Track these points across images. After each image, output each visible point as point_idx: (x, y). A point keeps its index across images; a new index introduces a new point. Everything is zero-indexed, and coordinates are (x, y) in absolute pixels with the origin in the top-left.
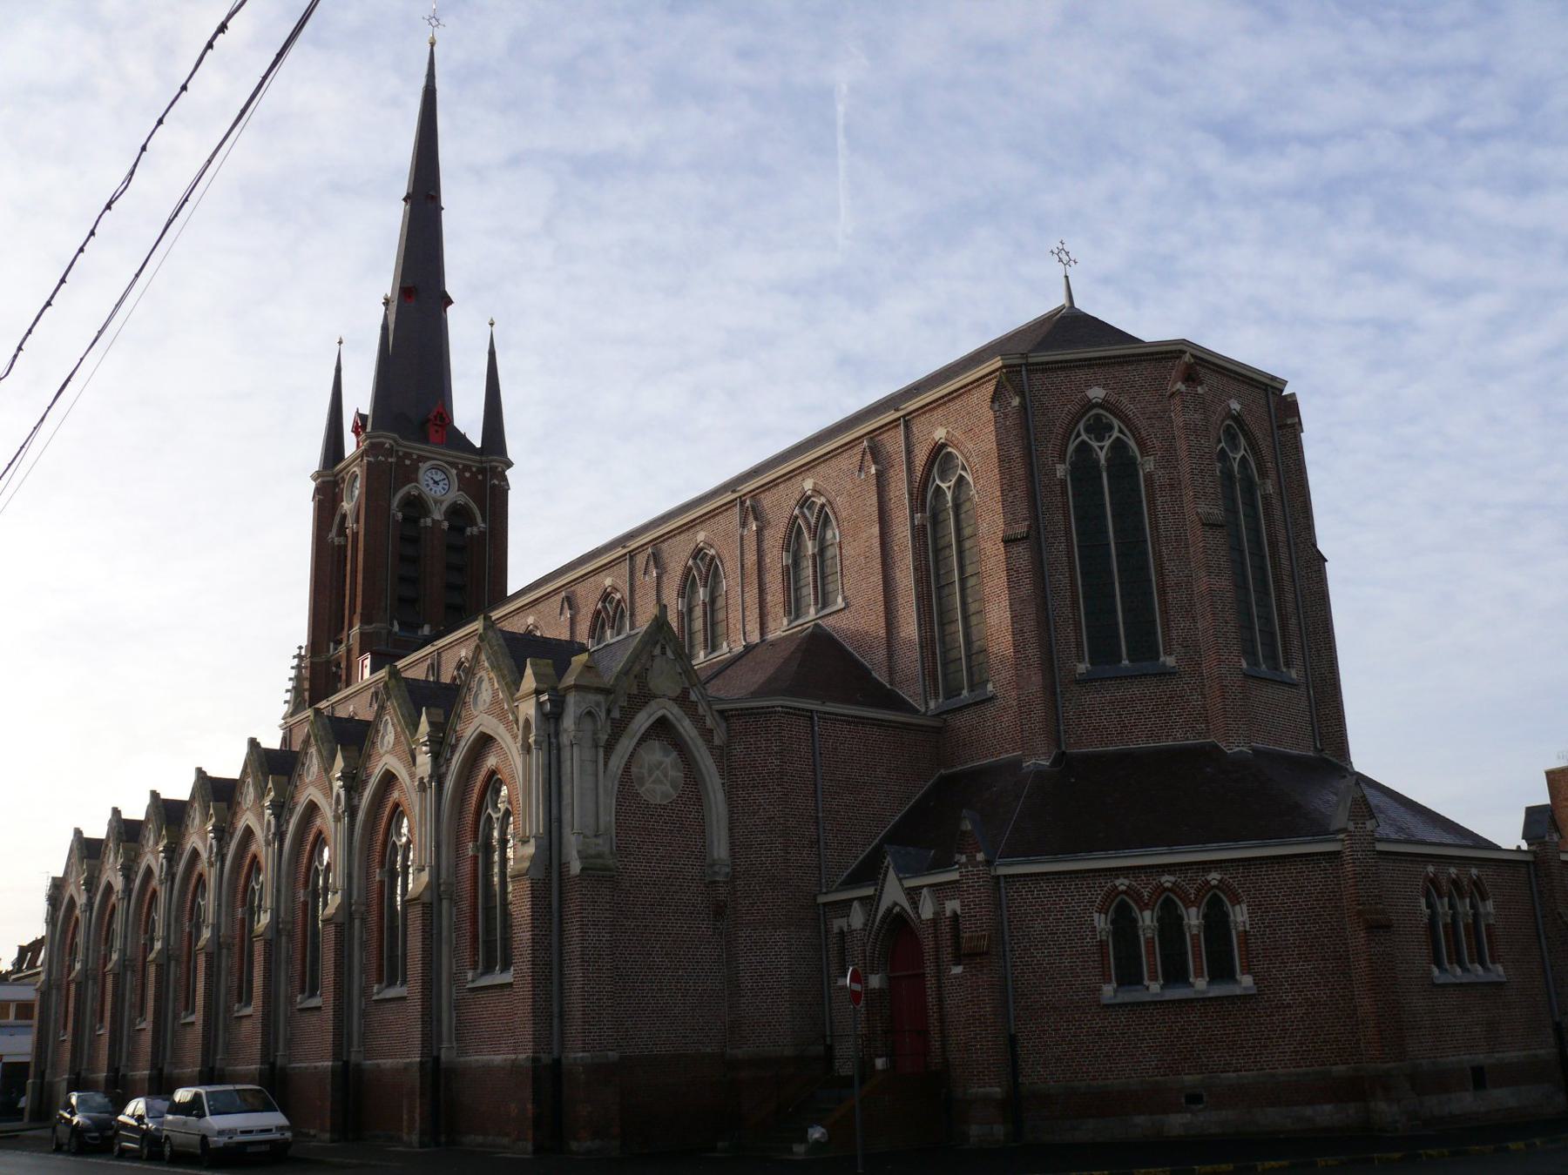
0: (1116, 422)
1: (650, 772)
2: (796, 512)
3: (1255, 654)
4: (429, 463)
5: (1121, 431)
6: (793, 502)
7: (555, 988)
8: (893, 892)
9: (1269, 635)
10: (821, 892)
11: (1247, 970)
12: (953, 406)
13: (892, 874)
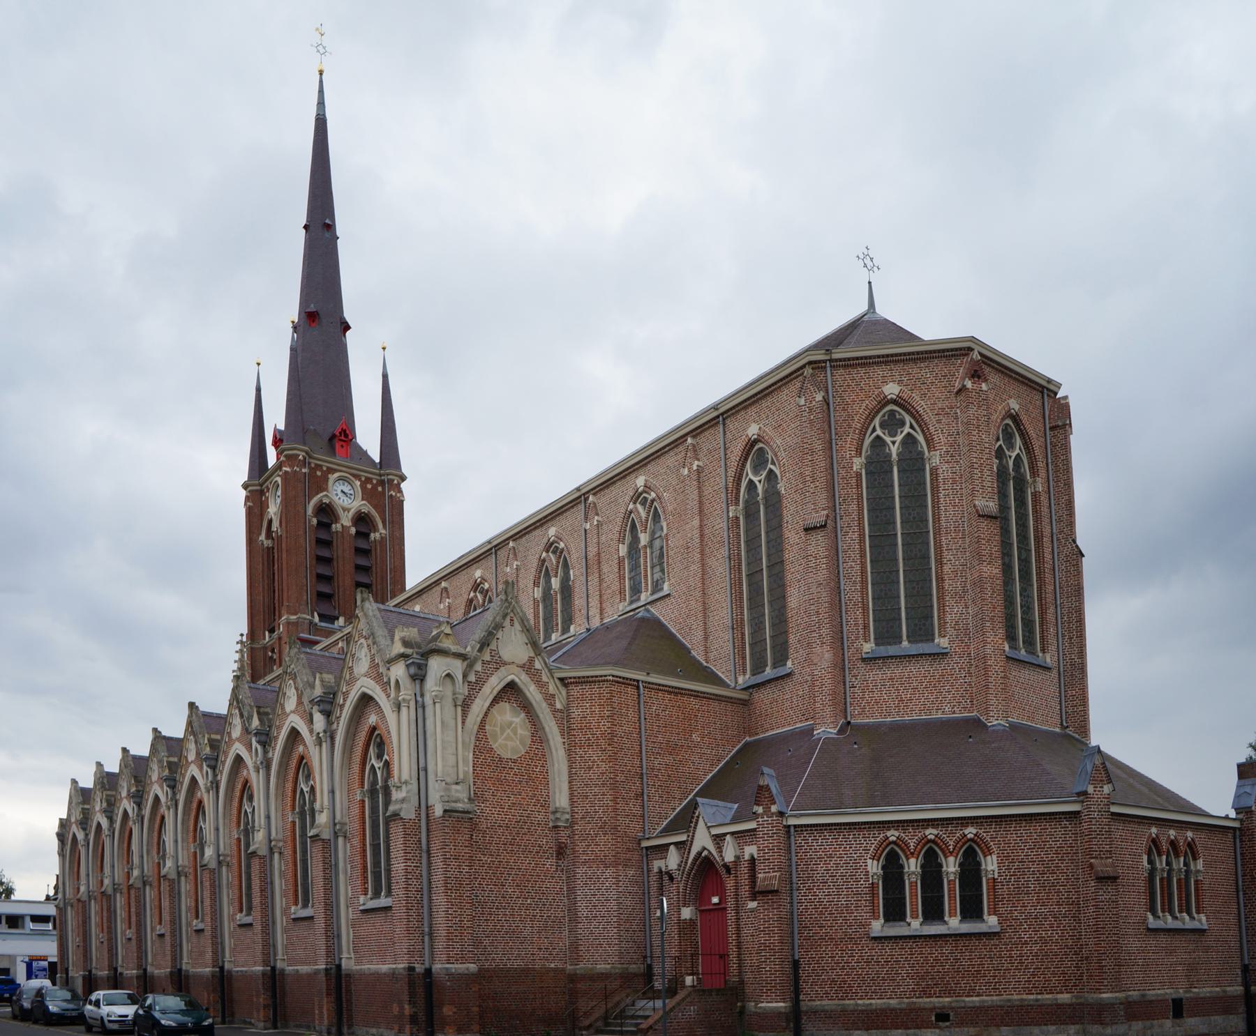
1: (503, 730)
2: (631, 506)
4: (337, 475)
5: (912, 427)
6: (627, 498)
7: (426, 910)
9: (1029, 624)
11: (993, 912)
12: (765, 403)
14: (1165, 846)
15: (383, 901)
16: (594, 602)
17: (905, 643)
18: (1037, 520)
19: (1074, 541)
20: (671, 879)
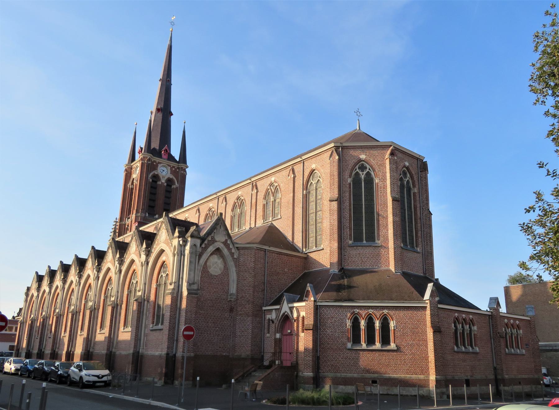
0: (368, 167)
3: (406, 242)
4: (162, 165)
8: (285, 308)
10: (264, 306)
13: (285, 302)
14: (461, 320)
15: (160, 326)
16: (253, 219)
17: (365, 242)
18: (415, 201)
19: (429, 209)
20: (273, 322)
